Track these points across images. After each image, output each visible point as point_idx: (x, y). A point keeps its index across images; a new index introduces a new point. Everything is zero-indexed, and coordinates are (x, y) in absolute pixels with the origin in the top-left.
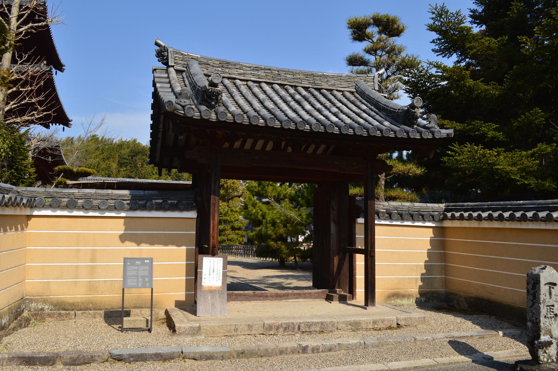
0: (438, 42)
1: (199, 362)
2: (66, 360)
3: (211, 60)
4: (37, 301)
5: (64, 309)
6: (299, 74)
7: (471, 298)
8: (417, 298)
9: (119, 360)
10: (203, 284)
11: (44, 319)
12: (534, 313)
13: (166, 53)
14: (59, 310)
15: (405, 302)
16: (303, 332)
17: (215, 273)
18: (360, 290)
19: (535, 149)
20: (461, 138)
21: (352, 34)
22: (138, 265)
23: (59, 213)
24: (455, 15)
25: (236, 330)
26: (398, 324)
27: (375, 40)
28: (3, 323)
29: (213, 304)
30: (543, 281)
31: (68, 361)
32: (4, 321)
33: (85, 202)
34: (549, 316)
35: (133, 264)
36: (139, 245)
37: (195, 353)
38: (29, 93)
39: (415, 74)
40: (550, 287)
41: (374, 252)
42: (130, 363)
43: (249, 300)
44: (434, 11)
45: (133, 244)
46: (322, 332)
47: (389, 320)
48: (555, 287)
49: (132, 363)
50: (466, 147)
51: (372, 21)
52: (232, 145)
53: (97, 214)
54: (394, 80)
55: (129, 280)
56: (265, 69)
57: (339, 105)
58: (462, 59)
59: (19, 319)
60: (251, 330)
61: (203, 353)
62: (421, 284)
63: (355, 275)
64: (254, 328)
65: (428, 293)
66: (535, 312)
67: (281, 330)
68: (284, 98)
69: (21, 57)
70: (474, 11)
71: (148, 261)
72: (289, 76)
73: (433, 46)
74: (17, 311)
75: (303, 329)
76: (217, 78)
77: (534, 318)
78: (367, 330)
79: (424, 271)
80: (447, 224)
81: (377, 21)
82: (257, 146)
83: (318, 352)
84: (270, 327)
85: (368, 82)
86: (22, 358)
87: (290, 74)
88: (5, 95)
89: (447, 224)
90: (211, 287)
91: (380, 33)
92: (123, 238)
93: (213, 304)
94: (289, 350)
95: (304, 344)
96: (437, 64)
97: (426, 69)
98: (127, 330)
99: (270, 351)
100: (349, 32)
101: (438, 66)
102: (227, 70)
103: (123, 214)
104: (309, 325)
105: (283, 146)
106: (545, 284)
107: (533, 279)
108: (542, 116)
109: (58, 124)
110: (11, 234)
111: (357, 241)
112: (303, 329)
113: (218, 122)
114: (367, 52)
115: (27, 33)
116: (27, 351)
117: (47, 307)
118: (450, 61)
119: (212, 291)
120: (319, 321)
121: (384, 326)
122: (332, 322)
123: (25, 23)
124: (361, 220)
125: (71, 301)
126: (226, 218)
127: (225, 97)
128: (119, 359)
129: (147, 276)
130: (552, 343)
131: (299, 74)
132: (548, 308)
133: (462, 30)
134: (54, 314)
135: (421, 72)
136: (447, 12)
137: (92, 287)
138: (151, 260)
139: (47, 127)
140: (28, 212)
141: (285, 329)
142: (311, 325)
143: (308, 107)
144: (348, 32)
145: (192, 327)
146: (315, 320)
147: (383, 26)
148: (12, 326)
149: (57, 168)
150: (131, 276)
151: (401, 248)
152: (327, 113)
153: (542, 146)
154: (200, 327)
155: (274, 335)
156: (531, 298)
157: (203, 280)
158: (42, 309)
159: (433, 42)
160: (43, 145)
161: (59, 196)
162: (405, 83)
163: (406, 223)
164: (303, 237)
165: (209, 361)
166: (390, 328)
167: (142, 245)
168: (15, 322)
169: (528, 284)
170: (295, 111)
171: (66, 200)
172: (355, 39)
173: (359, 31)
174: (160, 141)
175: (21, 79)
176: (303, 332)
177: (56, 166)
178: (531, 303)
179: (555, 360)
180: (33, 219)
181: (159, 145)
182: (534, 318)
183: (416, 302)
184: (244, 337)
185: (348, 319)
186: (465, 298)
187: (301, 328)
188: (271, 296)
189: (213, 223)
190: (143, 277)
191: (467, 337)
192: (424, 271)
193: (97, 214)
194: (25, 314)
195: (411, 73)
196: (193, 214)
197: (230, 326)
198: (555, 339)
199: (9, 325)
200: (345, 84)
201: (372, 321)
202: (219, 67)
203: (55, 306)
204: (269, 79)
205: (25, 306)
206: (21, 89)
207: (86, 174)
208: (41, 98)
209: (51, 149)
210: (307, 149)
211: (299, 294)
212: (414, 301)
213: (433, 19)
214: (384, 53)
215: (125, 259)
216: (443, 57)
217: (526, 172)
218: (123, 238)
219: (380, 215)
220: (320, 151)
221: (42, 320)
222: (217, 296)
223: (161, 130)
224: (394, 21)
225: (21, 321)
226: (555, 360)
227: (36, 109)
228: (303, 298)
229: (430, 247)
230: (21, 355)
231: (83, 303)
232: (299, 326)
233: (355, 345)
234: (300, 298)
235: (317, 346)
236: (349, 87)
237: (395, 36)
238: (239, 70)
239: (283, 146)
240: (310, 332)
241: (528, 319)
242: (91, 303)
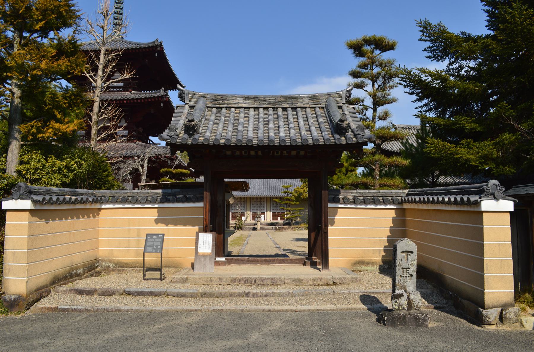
1: (177, 299)
3: (215, 96)
4: (106, 261)
5: (122, 267)
6: (280, 98)
8: (380, 265)
9: (130, 294)
11: (110, 272)
13: (184, 95)
15: (369, 268)
16: (259, 284)
17: (207, 244)
21: (354, 53)
23: (117, 206)
30: (399, 250)
34: (405, 275)
35: (152, 238)
36: (167, 225)
37: (174, 293)
43: (245, 264)
45: (164, 225)
47: (327, 279)
53: (140, 206)
56: (254, 98)
61: (179, 293)
62: (384, 254)
67: (242, 282)
73: (426, 54)
78: (308, 285)
79: (387, 244)
80: (406, 206)
81: (368, 42)
83: (257, 297)
84: (234, 280)
85: (337, 97)
86: (77, 290)
88: (96, 130)
89: (406, 206)
90: (204, 253)
92: (157, 221)
95: (247, 291)
98: (148, 279)
99: (223, 294)
102: (226, 102)
103: (156, 206)
104: (263, 280)
106: (402, 252)
108: (510, 109)
110: (83, 221)
111: (329, 220)
112: (258, 282)
119: (205, 256)
122: (280, 278)
125: (126, 262)
128: (129, 293)
131: (280, 98)
132: (405, 270)
138: (163, 235)
140: (98, 206)
141: (245, 282)
153: (506, 136)
154: (187, 278)
155: (238, 285)
158: (109, 266)
159: (425, 50)
161: (118, 195)
163: (369, 206)
165: (183, 298)
166: (327, 285)
167: (169, 225)
173: (357, 49)
176: (259, 284)
180: (102, 210)
183: (379, 268)
184: (216, 285)
185: (293, 277)
187: (257, 281)
190: (157, 246)
191: (380, 293)
192: (387, 244)
193: (353, 206)
197: (207, 278)
199: (84, 274)
200: (317, 101)
202: (220, 100)
203: (116, 264)
204: (257, 105)
211: (283, 260)
212: (378, 268)
213: (421, 31)
217: (486, 159)
218: (157, 221)
221: (109, 273)
222: (208, 259)
229: (392, 225)
231: (133, 263)
232: (255, 280)
233: (285, 293)
236: (320, 104)
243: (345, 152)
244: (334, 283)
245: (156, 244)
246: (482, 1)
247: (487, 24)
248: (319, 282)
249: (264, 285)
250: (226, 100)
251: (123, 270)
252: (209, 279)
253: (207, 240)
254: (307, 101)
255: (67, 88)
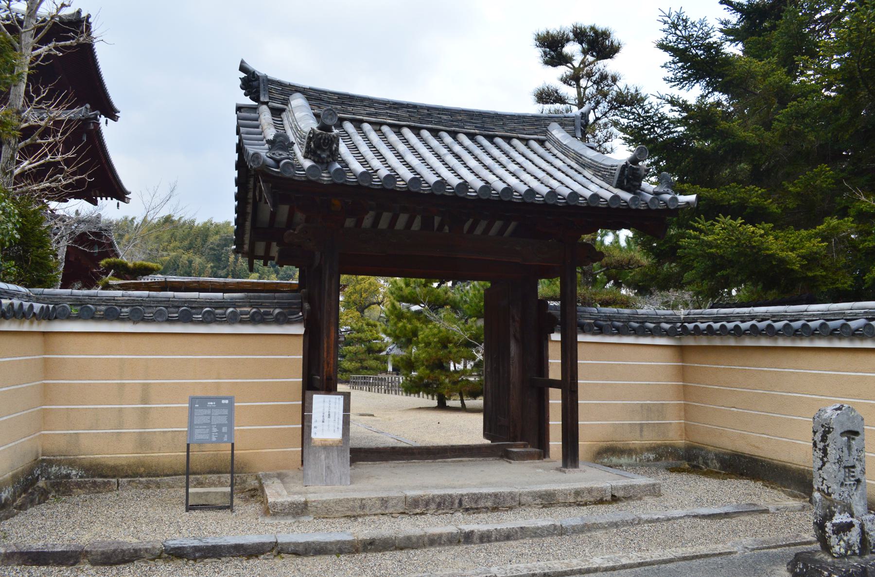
0: (673, 66)
2: (95, 557)
4: (59, 463)
7: (725, 454)
10: (313, 436)
12: (824, 479)
13: (255, 83)
14: (93, 477)
17: (332, 418)
18: (555, 443)
19: (821, 227)
20: (708, 209)
22: (212, 408)
24: (698, 26)
25: (363, 507)
26: (613, 496)
27: (576, 64)
28: (3, 498)
29: (328, 467)
31: (99, 558)
32: (4, 495)
33: (131, 311)
35: (203, 406)
37: (297, 544)
38: (53, 149)
39: (639, 114)
40: (849, 438)
41: (576, 384)
42: (195, 560)
44: (666, 19)
46: (495, 509)
48: (856, 438)
49: (198, 560)
50: (718, 222)
51: (571, 35)
52: (359, 222)
54: (605, 125)
55: (197, 431)
57: (521, 159)
58: (709, 93)
59: (30, 491)
60: (386, 507)
63: (548, 420)
64: (390, 504)
65: (659, 446)
66: (826, 477)
67: (433, 506)
68: (436, 150)
69: (37, 92)
70: (725, 23)
71: (227, 402)
72: (445, 117)
74: (27, 479)
75: (466, 504)
76: (329, 117)
77: (824, 487)
81: (580, 35)
82: (381, 222)
84: (415, 502)
86: (27, 553)
87: (446, 115)
90: (325, 441)
91: (585, 52)
93: (328, 467)
94: (444, 539)
96: (672, 98)
97: (656, 107)
99: (414, 540)
100: (538, 52)
101: (673, 102)
102: (350, 109)
105: (436, 224)
107: (823, 426)
109: (109, 198)
111: (550, 369)
112: (466, 504)
113: (334, 185)
114: (565, 83)
115: (48, 57)
116: (37, 545)
117: (74, 472)
118: (693, 94)
119: (327, 447)
120: (492, 490)
121: (592, 499)
122: (511, 493)
123: (43, 41)
124: (556, 337)
125: (111, 463)
126: (360, 335)
127: (343, 148)
129: (224, 425)
130: (853, 526)
133: (708, 47)
134: (86, 483)
135: (647, 112)
136: (685, 21)
137: (143, 442)
138: (231, 399)
139: (95, 203)
141: (439, 505)
142: (479, 498)
143: (472, 163)
144: (537, 53)
145: (293, 503)
146: (485, 490)
147: (589, 43)
148: (19, 501)
149: (103, 262)
150: (200, 425)
151: (619, 380)
152: (500, 171)
154: (306, 503)
155: (422, 514)
156: (821, 454)
157: (313, 430)
158: (68, 476)
159: (665, 66)
160: (83, 228)
162: (623, 130)
164: (472, 363)
168: (23, 495)
169: (815, 432)
170: (451, 169)
171: (103, 308)
172: (546, 63)
173: (552, 48)
174: (249, 218)
175: (40, 126)
177: (102, 259)
178: (820, 463)
179: (857, 551)
181: (248, 224)
182: (824, 487)
186: (716, 455)
187: (464, 503)
188: (419, 453)
189: (328, 343)
190: (220, 427)
194: (41, 483)
195: (633, 113)
196: (299, 329)
198: (857, 518)
199: (14, 501)
201: (573, 491)
202: (337, 104)
205: (41, 471)
206: (39, 141)
207: (147, 271)
208: (69, 155)
209: (94, 234)
210: (473, 228)
214: (590, 84)
215: (193, 400)
216: (680, 89)
219: (585, 328)
220: (493, 231)
223: (251, 201)
224: (605, 35)
225: (32, 494)
226: (857, 551)
227: (61, 171)
228: (468, 457)
230: (25, 549)
231: (129, 466)
234: (463, 456)
235: (488, 531)
236: (536, 134)
237: (606, 58)
238: (368, 109)
239: (436, 224)
240: (477, 509)
241: (816, 487)
242: (143, 466)
243: (417, 229)
244: (615, 499)
245: (216, 420)
246: (721, 3)
247: (84, 14)
248: (587, 498)
249: (477, 510)
250: (350, 105)
251: (105, 483)
252: (357, 504)
253: (332, 410)
254: (513, 125)
255: (589, 50)
